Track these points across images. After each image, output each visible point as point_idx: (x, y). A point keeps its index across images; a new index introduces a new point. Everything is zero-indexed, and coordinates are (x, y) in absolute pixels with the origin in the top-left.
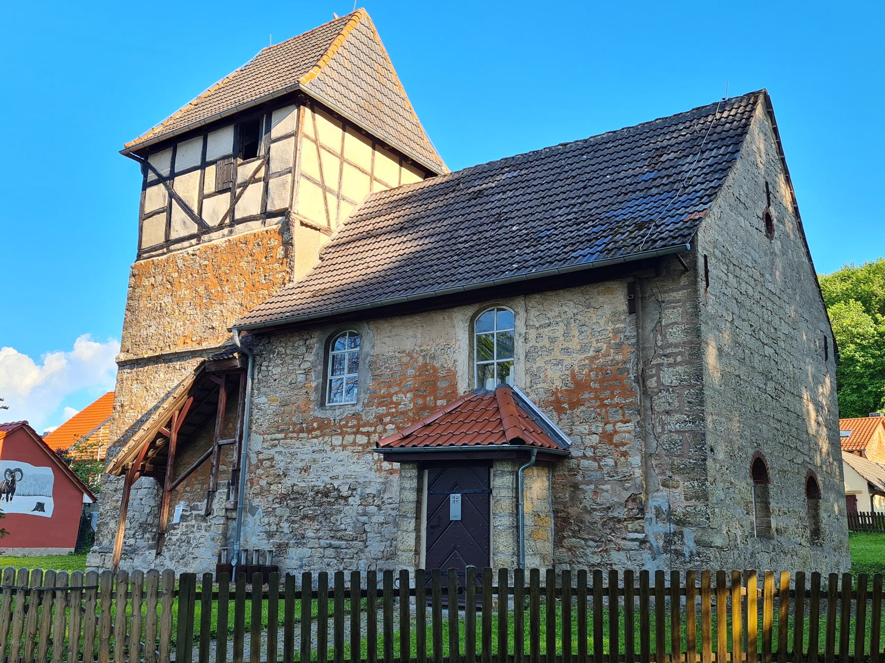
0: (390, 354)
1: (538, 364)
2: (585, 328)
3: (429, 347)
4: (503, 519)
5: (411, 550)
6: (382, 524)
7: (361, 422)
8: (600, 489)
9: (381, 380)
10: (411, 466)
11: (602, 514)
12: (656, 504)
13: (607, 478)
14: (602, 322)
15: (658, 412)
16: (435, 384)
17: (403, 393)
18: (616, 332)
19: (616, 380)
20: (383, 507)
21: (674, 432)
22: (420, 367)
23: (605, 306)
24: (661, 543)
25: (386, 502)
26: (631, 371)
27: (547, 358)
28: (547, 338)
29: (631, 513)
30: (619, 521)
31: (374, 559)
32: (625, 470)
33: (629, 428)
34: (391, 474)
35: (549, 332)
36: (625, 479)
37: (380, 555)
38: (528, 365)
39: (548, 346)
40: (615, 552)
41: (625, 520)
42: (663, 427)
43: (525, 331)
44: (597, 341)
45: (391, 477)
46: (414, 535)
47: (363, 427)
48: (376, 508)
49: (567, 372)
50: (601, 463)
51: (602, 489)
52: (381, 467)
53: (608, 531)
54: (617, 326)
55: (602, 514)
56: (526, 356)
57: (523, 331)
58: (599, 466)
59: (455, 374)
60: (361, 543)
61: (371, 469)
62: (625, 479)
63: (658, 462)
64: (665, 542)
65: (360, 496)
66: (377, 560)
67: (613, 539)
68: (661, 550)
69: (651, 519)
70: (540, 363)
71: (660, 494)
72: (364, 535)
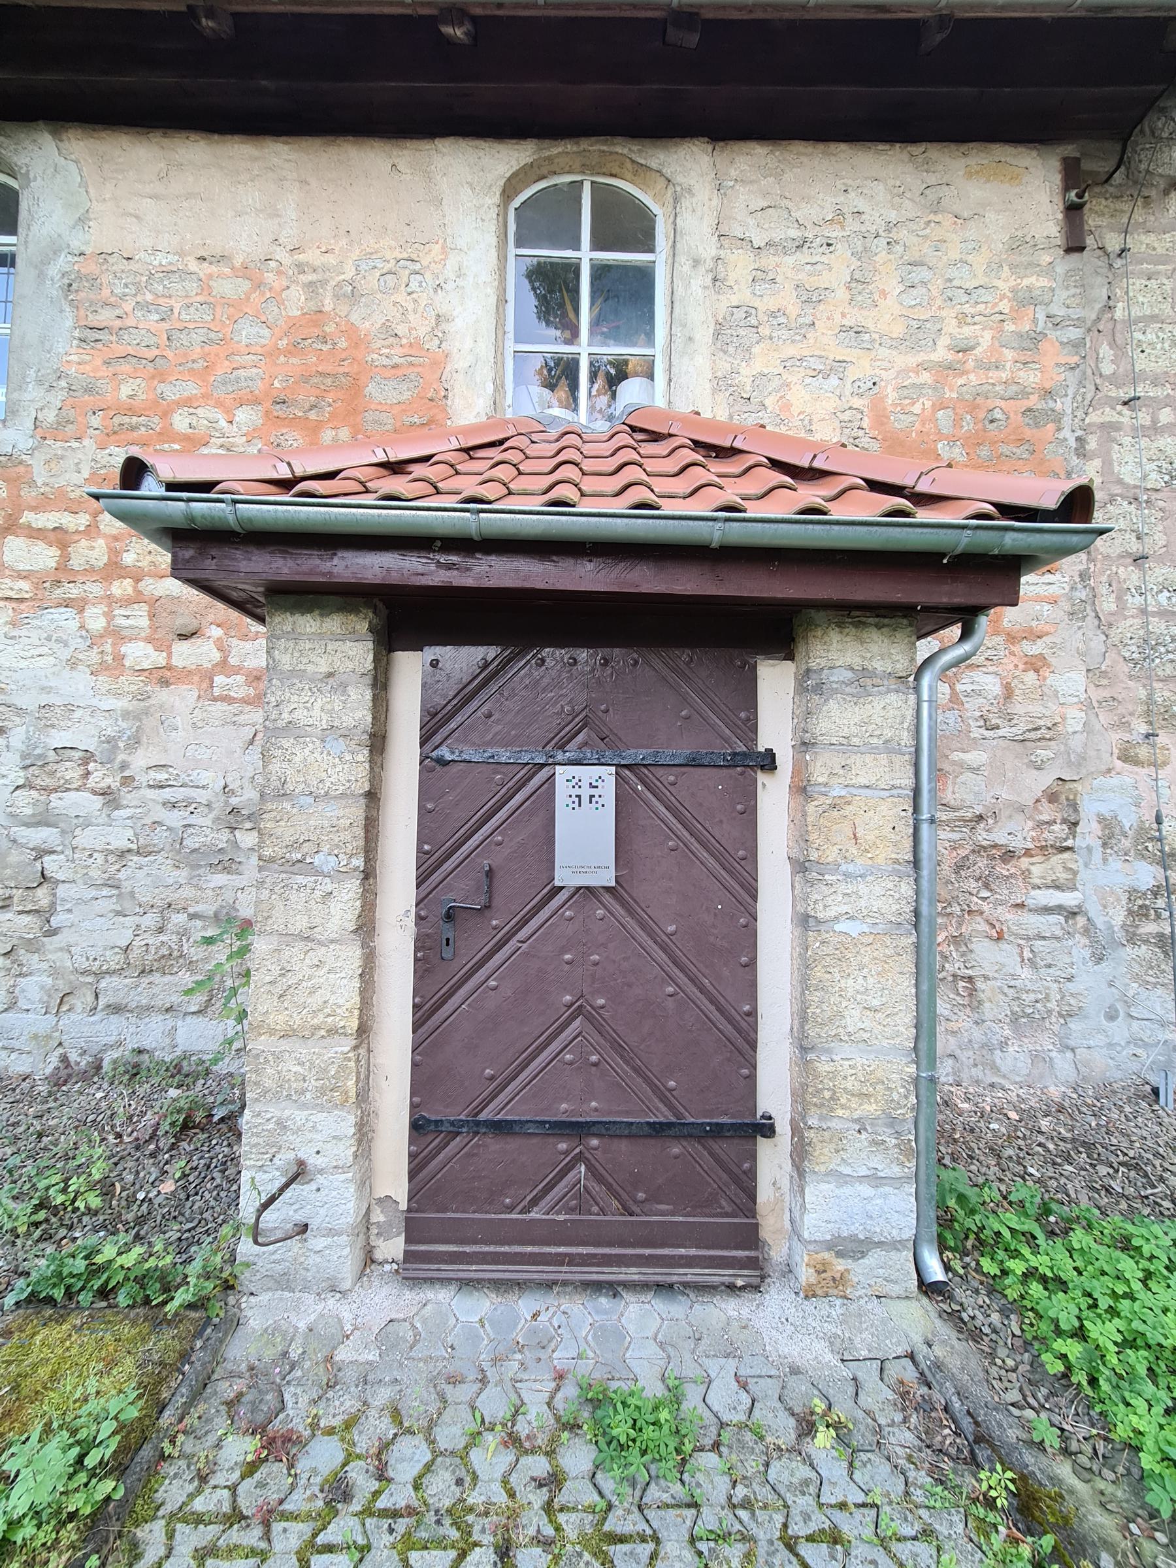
0: (162, 259)
1: (758, 366)
2: (922, 273)
3: (331, 259)
4: (863, 889)
5: (332, 1032)
6: (122, 854)
7: (28, 495)
8: (954, 763)
9: (121, 350)
10: (334, 623)
11: (956, 836)
12: (1104, 809)
13: (977, 733)
14: (979, 261)
15: (1107, 557)
16: (355, 388)
17: (219, 404)
18: (1026, 300)
19: (1021, 441)
20: (128, 798)
21: (1154, 614)
22: (293, 324)
23: (991, 216)
24: (1118, 917)
25: (142, 779)
26: (1067, 421)
27: (791, 351)
28: (789, 286)
29: (1046, 835)
30: (1009, 855)
31: (85, 972)
32: (1036, 709)
33: (1051, 589)
34: (165, 683)
35: (796, 268)
36: (1038, 735)
37: (114, 960)
38: (724, 366)
39: (793, 310)
40: (987, 943)
41: (1028, 853)
42: (1119, 598)
43: (714, 252)
44: (962, 319)
45: (163, 696)
46: (352, 955)
47: (35, 509)
48: (98, 801)
49: (857, 402)
50: (959, 687)
51: (961, 764)
52: (119, 658)
53: (972, 885)
54: (1026, 282)
55: (956, 836)
56: (717, 335)
57: (708, 249)
58: (954, 694)
59: (439, 363)
60: (27, 919)
61: (72, 664)
62: (1038, 735)
63: (1106, 693)
64: (1130, 912)
65: (24, 757)
66: (100, 974)
67: (986, 907)
68: (1120, 935)
69: (1089, 849)
70: (764, 360)
71: (1115, 781)
72: (41, 893)
